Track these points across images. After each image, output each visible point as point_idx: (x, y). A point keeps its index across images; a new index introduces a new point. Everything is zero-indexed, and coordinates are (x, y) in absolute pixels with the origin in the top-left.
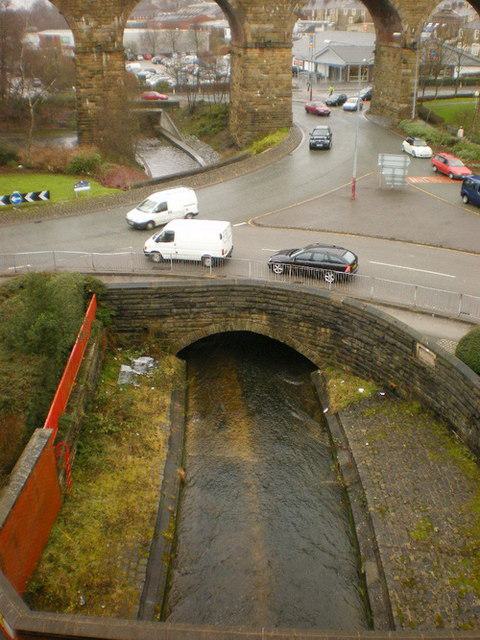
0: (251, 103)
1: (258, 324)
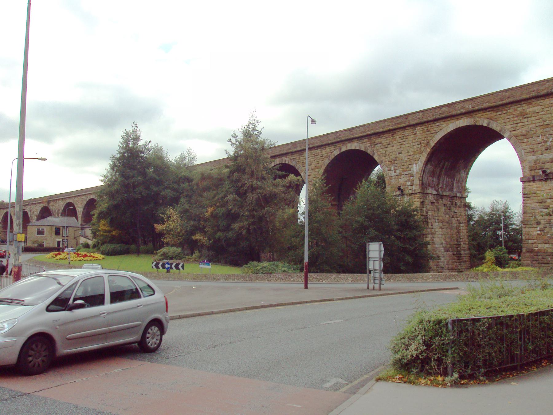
0: (530, 241)
1: (354, 146)
